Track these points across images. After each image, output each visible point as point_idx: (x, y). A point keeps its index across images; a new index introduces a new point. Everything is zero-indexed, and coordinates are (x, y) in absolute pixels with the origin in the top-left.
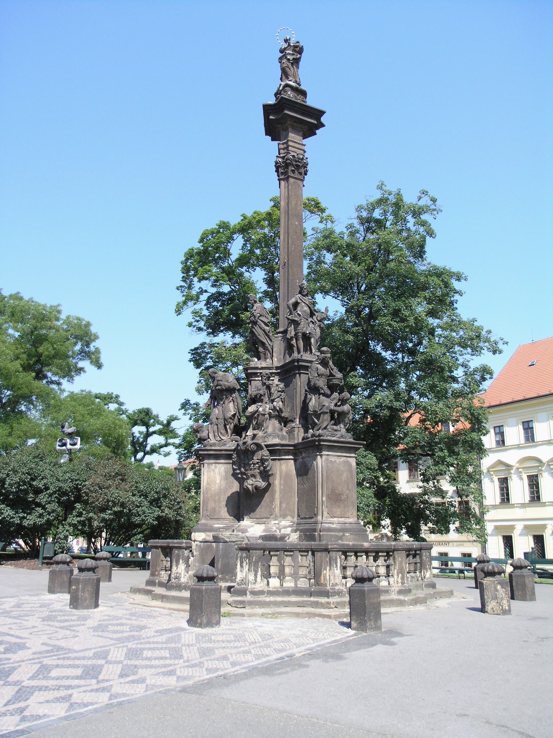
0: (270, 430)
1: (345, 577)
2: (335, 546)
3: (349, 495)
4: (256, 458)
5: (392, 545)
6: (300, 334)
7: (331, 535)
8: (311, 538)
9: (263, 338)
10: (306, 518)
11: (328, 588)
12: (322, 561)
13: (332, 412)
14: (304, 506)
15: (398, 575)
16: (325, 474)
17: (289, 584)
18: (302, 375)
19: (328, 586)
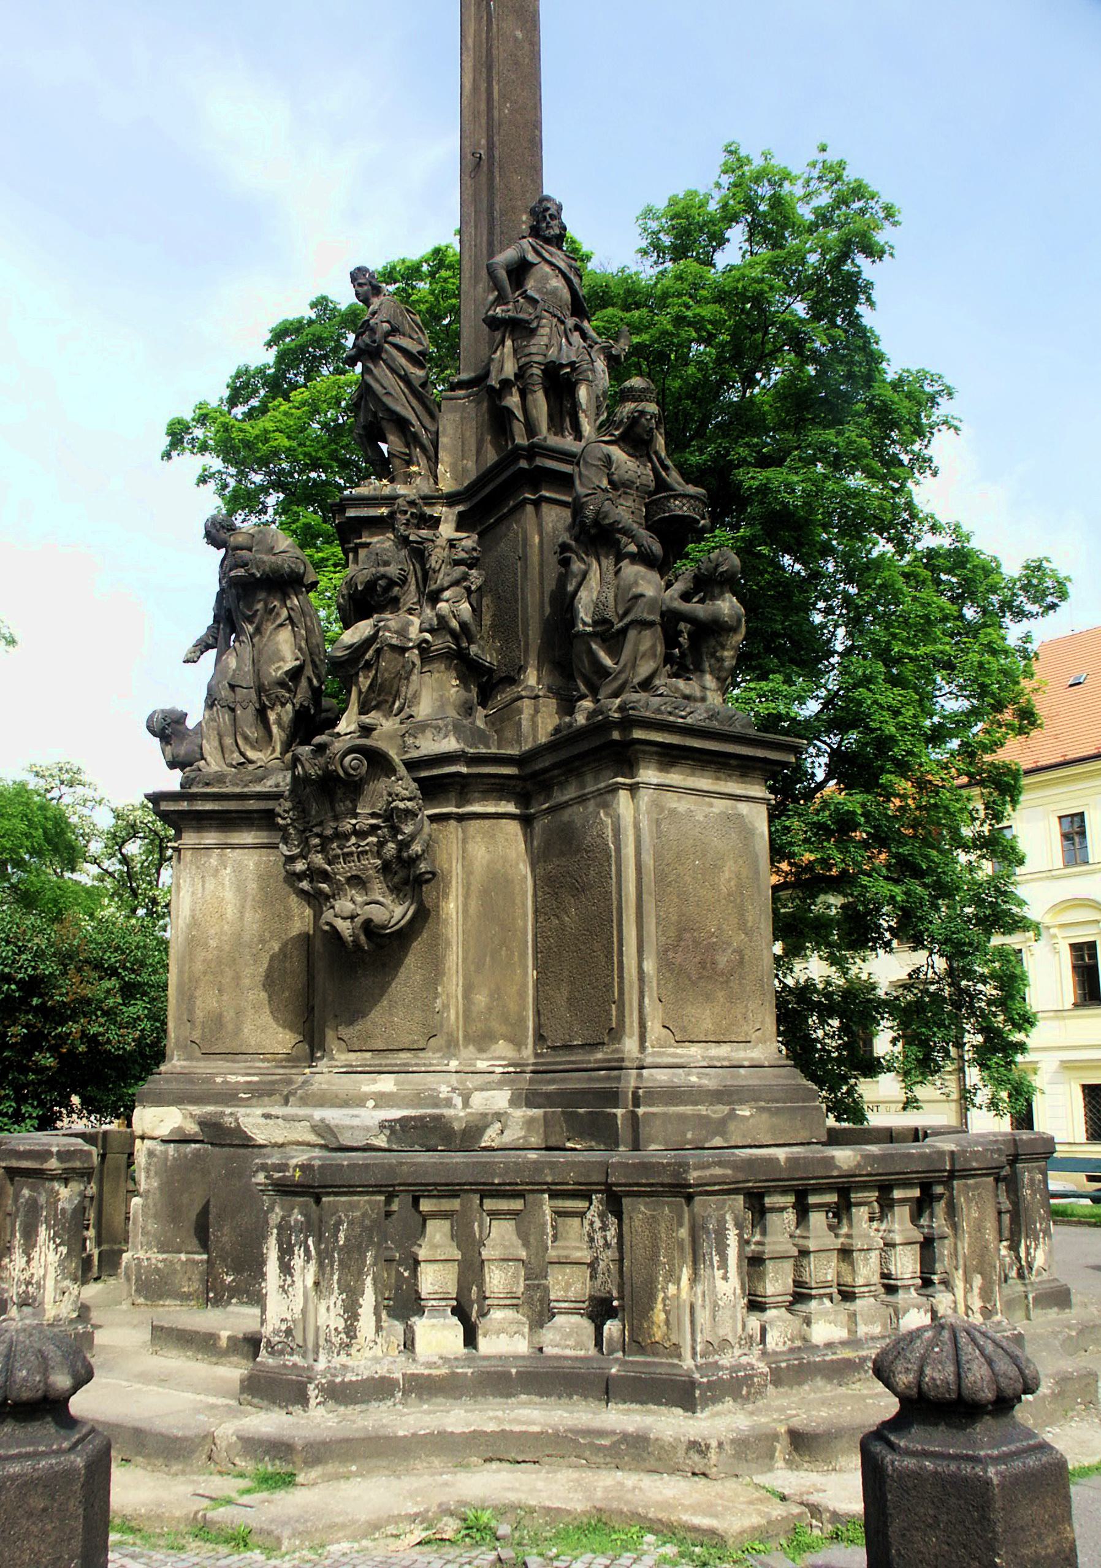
0: (424, 709)
1: (756, 1305)
2: (718, 1171)
3: (748, 952)
4: (365, 815)
5: (941, 1153)
6: (536, 371)
7: (682, 1118)
8: (601, 1131)
9: (404, 406)
10: (568, 1047)
11: (688, 1363)
12: (655, 1238)
13: (670, 619)
14: (561, 997)
15: (967, 1280)
16: (648, 860)
17: (505, 1339)
18: (545, 508)
19: (687, 1352)
